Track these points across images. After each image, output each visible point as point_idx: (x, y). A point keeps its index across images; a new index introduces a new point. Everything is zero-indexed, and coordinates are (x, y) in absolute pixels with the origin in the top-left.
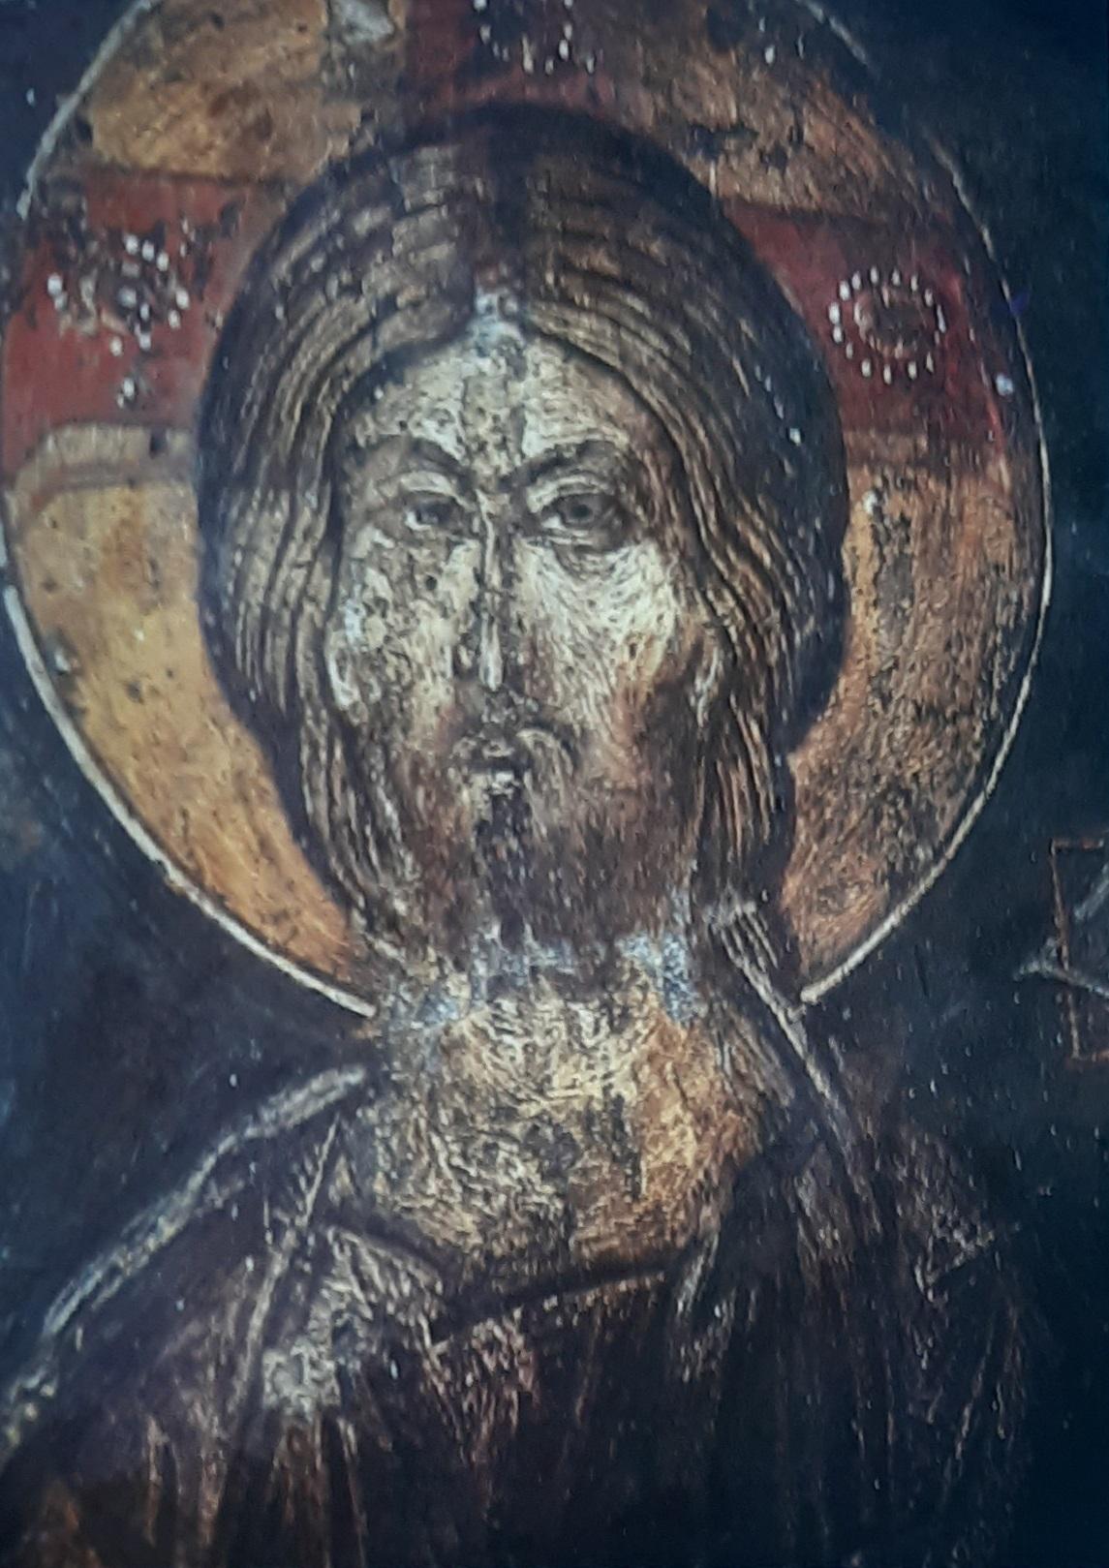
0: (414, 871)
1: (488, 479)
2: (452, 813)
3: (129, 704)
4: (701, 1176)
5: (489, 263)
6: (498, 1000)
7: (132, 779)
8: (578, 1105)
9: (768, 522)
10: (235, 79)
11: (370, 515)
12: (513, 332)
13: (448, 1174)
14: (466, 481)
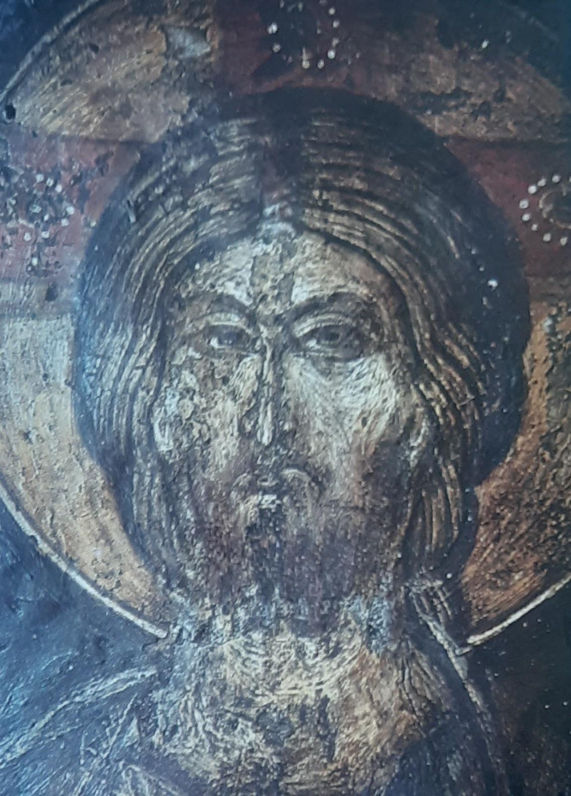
0: (201, 553)
1: (267, 317)
2: (233, 519)
3: (23, 443)
4: (379, 750)
5: (271, 188)
6: (250, 633)
7: (20, 486)
8: (298, 701)
9: (470, 340)
10: (106, 81)
11: (185, 341)
12: (288, 228)
13: (204, 736)
14: (252, 318)
